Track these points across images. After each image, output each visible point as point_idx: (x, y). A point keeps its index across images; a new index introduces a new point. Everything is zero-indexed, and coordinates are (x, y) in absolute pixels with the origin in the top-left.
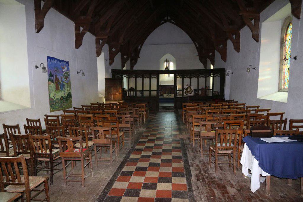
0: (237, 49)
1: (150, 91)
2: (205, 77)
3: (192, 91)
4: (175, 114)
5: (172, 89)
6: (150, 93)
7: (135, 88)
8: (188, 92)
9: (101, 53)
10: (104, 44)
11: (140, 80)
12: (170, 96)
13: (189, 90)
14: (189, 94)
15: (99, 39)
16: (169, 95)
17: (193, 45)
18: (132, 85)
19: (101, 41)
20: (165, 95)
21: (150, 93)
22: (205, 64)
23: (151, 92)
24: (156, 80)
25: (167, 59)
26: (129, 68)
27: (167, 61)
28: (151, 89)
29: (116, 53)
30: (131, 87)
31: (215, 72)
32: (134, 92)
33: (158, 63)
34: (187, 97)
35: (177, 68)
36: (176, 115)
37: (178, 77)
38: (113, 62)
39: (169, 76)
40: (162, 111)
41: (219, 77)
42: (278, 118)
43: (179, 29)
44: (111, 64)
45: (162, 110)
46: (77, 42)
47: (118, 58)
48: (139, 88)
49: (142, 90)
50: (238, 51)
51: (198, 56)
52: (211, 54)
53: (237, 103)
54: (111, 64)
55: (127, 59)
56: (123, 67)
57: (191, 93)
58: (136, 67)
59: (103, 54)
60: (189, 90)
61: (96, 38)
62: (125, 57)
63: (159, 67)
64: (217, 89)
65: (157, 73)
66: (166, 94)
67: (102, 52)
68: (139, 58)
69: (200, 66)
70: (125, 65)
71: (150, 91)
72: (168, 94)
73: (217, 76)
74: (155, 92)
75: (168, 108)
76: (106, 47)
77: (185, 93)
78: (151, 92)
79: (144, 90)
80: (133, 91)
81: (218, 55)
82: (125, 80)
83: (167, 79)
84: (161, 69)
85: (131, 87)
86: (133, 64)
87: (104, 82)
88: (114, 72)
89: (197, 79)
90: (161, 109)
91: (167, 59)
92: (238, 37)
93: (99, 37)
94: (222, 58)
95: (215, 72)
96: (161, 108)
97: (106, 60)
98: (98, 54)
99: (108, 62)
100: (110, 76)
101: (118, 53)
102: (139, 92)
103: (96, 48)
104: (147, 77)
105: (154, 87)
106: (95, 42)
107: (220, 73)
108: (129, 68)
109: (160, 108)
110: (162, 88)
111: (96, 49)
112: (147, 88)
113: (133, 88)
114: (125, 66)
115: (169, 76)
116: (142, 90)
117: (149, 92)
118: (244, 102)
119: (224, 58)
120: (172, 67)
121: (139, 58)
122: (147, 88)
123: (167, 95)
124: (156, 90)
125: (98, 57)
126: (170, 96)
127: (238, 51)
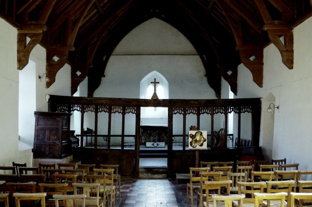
0: (289, 62)
1: (123, 136)
2: (211, 114)
3: (205, 141)
4: (171, 185)
5: (162, 133)
6: (123, 139)
7: (94, 130)
8: (196, 141)
9: (27, 62)
10: (35, 45)
11: (103, 116)
12: (153, 145)
13: (198, 138)
14: (198, 147)
15: (25, 35)
16: (155, 145)
17: (198, 58)
18: (89, 124)
19: (28, 40)
20: (149, 144)
21: (123, 139)
22: (218, 89)
23: (125, 138)
24: (134, 116)
25: (155, 79)
26: (85, 95)
27: (155, 83)
28: (125, 134)
29: (60, 65)
30: (88, 129)
31: (239, 105)
32: (93, 138)
33: (136, 85)
34: (194, 151)
35: (80, 95)
36: (173, 186)
37: (175, 112)
38: (54, 81)
39: (155, 110)
40: (144, 177)
41: (250, 114)
42: (293, 170)
43: (175, 31)
44: (49, 85)
45: (144, 174)
46: (19, 61)
47: (64, 74)
48: (103, 130)
49: (107, 134)
50: (291, 67)
51: (206, 76)
52: (230, 73)
53: (297, 169)
54: (49, 85)
55: (82, 78)
56: (74, 90)
57: (202, 145)
58: (99, 93)
59: (31, 64)
60: (198, 138)
61: (18, 34)
62: (56, 59)
63: (139, 94)
64: (247, 135)
65: (137, 105)
66: (150, 142)
67: (29, 60)
68: (104, 76)
69: (209, 94)
70: (78, 88)
71: (123, 136)
72: (154, 141)
73: (246, 113)
74: (132, 139)
75: (156, 170)
76: (39, 52)
77: (191, 145)
78: (125, 138)
79: (112, 134)
80: (92, 136)
81: (244, 74)
82: (76, 115)
83: (154, 116)
84: (142, 97)
85: (88, 129)
86: (93, 86)
87: (33, 119)
88: (54, 101)
89: (122, 115)
90: (142, 173)
91: (155, 79)
92: (290, 40)
93: (26, 32)
94: (254, 80)
95: (239, 105)
96: (144, 170)
97: (40, 77)
98: (22, 63)
99: (45, 80)
100: (45, 109)
101: (64, 65)
102: (102, 138)
103: (19, 51)
104: (117, 111)
105: (131, 128)
106: (16, 40)
107: (253, 106)
108: (85, 95)
109: (141, 170)
110: (146, 132)
111: (18, 53)
112: (116, 130)
113: (92, 130)
114: (77, 90)
115: (155, 110)
116: (107, 134)
117: (121, 138)
118: (296, 163)
119: (258, 79)
120: (163, 94)
121: (104, 76)
122: (116, 130)
123: (153, 145)
124: (134, 134)
125: (21, 69)
126: (158, 145)
127: (291, 67)
